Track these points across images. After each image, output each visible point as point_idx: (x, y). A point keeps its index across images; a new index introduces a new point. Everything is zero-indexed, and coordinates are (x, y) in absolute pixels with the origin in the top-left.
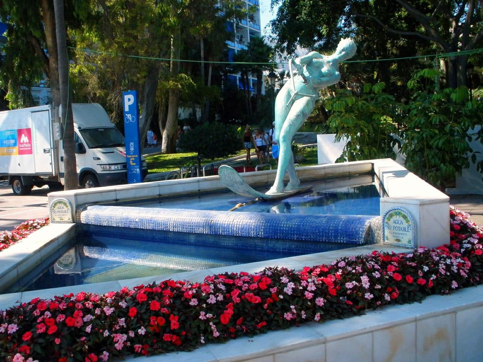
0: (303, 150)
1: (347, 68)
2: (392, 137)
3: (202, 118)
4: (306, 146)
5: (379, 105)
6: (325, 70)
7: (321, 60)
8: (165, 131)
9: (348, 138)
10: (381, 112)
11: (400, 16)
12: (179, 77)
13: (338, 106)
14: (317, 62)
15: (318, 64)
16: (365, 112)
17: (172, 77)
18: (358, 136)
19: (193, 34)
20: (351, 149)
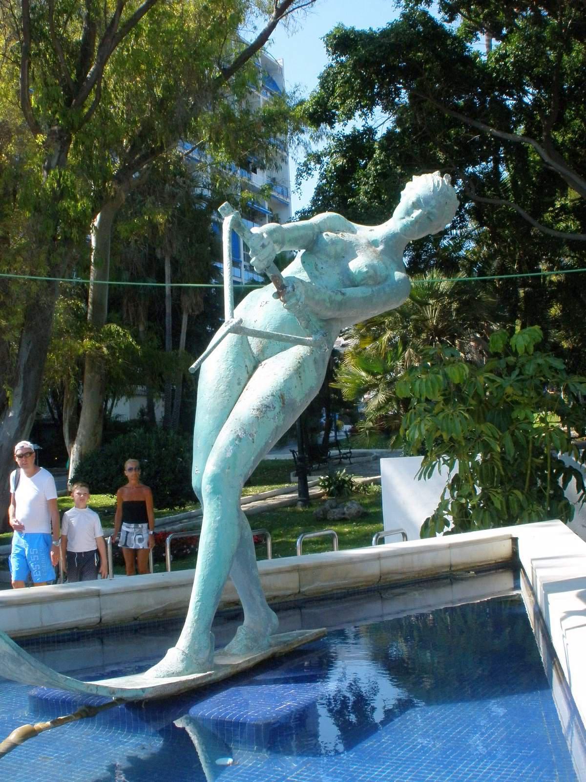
0: (364, 489)
1: (457, 310)
2: (561, 462)
3: (165, 419)
4: (372, 481)
5: (527, 383)
6: (358, 264)
7: (348, 237)
8: (75, 446)
9: (451, 467)
10: (535, 401)
11: (563, 207)
12: (105, 331)
13: (426, 386)
14: (334, 242)
15: (339, 248)
16: (495, 402)
17: (91, 330)
18: (477, 462)
19: (126, 234)
20: (459, 496)
